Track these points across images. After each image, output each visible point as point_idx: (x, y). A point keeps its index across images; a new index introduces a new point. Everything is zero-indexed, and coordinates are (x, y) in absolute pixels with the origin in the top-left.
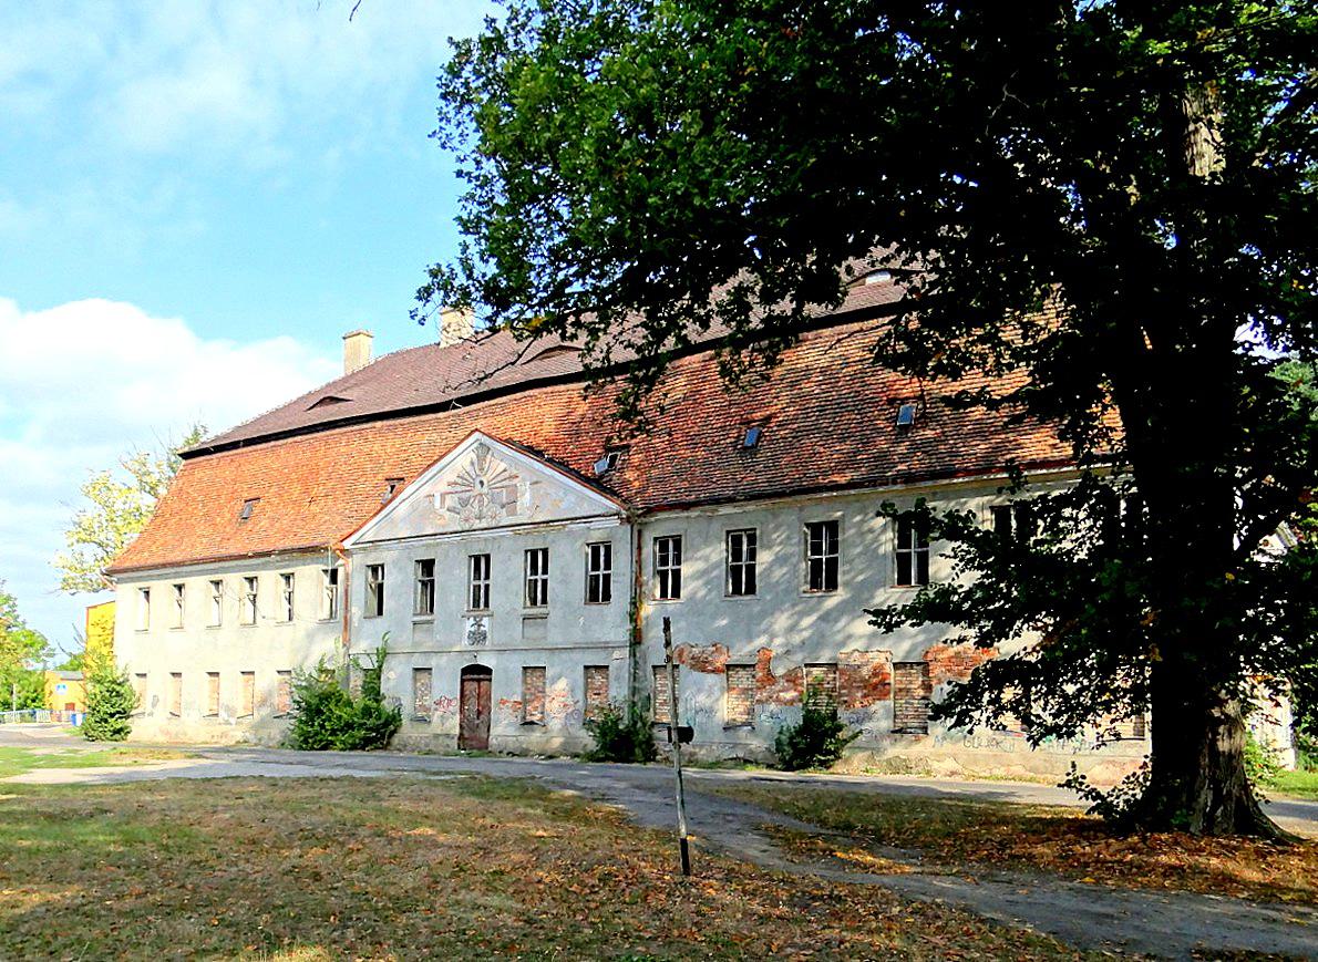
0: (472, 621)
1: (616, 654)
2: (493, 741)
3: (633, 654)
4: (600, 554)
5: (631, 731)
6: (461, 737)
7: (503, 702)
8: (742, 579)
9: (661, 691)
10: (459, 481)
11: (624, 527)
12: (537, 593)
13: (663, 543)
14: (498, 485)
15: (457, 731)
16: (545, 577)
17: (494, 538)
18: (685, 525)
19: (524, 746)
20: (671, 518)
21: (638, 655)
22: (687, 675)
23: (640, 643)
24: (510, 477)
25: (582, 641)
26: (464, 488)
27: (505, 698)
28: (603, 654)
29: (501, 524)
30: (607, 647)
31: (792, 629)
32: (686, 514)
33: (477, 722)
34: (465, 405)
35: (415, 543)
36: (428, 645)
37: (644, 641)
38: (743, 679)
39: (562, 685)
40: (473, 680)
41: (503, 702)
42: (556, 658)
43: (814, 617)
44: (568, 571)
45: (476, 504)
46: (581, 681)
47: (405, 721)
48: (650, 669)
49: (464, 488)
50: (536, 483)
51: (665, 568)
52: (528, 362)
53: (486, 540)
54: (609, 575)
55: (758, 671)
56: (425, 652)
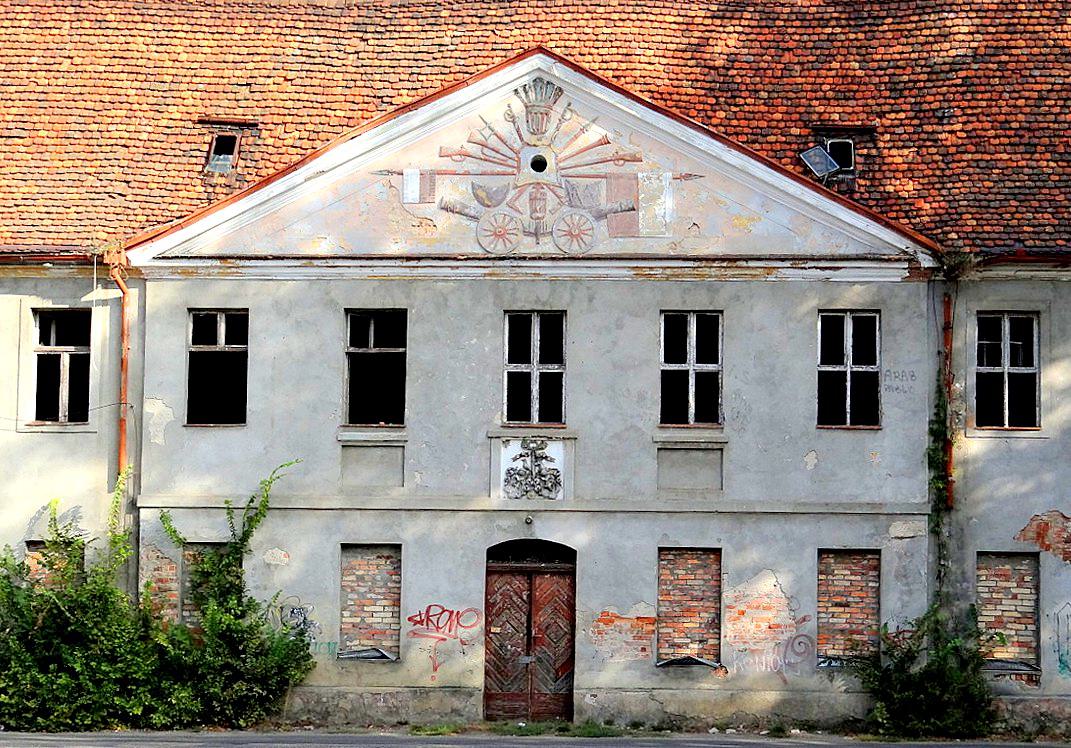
0: (515, 448)
1: (899, 528)
2: (583, 698)
3: (935, 532)
4: (849, 339)
5: (936, 674)
6: (488, 696)
7: (607, 619)
9: (989, 601)
11: (912, 285)
12: (689, 398)
13: (989, 325)
15: (478, 680)
18: (1048, 293)
20: (1016, 279)
21: (945, 531)
23: (949, 509)
24: (620, 159)
25: (813, 499)
26: (488, 167)
27: (612, 610)
28: (867, 528)
29: (593, 252)
30: (877, 514)
32: (1053, 274)
33: (527, 660)
35: (353, 270)
36: (397, 496)
37: (957, 506)
38: (253, 524)
39: (767, 586)
40: (513, 572)
41: (607, 619)
42: (749, 529)
44: (770, 363)
45: (523, 203)
46: (812, 579)
47: (320, 654)
48: (971, 561)
49: (488, 167)
50: (688, 176)
51: (997, 370)
53: (553, 281)
56: (409, 510)
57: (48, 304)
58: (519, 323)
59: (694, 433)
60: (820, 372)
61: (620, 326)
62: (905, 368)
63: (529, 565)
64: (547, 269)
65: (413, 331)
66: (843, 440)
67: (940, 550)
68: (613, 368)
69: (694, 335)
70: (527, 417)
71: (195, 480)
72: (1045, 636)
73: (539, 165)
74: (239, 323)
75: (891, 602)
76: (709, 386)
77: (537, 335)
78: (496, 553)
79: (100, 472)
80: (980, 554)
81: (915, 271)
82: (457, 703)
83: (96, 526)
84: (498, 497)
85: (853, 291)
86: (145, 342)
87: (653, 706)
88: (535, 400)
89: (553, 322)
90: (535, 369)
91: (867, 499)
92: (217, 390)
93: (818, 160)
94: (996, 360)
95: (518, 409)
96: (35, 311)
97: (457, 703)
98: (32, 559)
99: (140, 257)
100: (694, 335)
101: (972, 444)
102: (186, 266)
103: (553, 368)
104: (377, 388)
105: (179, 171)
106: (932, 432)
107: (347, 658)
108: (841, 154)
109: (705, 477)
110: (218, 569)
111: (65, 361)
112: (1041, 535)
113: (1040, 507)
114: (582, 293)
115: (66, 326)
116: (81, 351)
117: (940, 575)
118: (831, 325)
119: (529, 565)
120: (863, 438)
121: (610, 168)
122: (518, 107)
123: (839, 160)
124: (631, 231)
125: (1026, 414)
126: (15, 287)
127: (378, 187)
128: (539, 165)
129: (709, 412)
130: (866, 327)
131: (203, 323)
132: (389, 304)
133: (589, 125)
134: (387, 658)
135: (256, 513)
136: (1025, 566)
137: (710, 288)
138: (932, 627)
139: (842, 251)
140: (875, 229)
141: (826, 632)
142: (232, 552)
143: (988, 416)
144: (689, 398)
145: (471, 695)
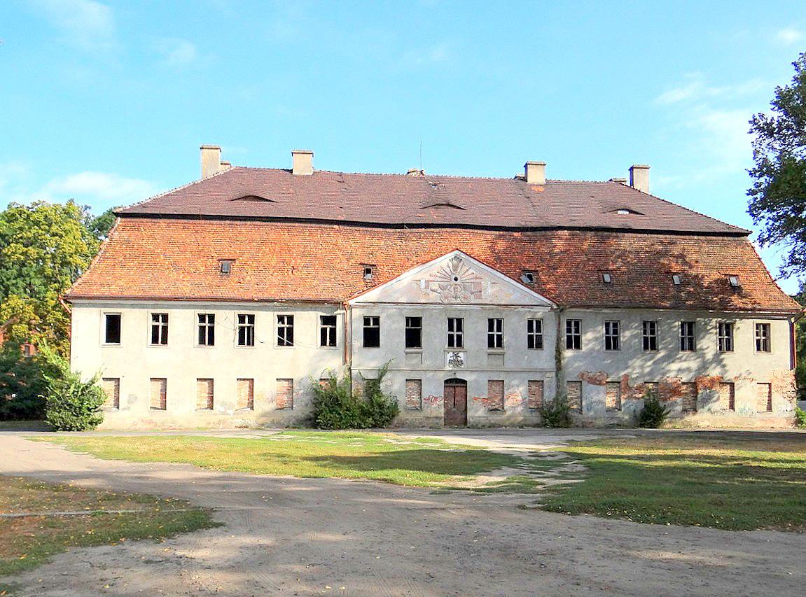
0: (451, 354)
1: (548, 375)
3: (557, 376)
4: (534, 326)
7: (476, 399)
8: (612, 343)
10: (439, 275)
12: (495, 341)
13: (569, 323)
14: (467, 281)
16: (203, 324)
17: (466, 310)
19: (492, 422)
21: (559, 375)
22: (587, 387)
24: (476, 278)
26: (442, 279)
30: (543, 371)
31: (642, 367)
33: (454, 409)
34: (409, 228)
35: (408, 306)
43: (652, 361)
44: (515, 333)
47: (400, 408)
49: (442, 279)
50: (494, 283)
52: (270, 201)
53: (460, 310)
54: (489, 331)
55: (622, 386)
57: (325, 314)
58: (451, 321)
59: (496, 350)
60: (489, 334)
61: (478, 322)
62: (549, 334)
63: (456, 384)
64: (459, 307)
65: (423, 323)
66: (534, 352)
67: (558, 380)
68: (475, 333)
69: (495, 324)
70: (453, 346)
71: (366, 362)
72: (583, 404)
73: (456, 279)
74: (376, 320)
75: (546, 394)
76: (500, 338)
77: (456, 324)
78: (446, 382)
79: (341, 360)
80: (568, 381)
81: (552, 309)
82: (437, 421)
83: (340, 377)
84: (448, 368)
85: (540, 313)
86: (351, 323)
87: (488, 421)
88: (455, 341)
89: (460, 321)
90: (495, 333)
91: (541, 367)
92: (371, 338)
93: (524, 278)
94: (571, 332)
95: (451, 344)
96: (321, 316)
97: (437, 421)
98: (323, 383)
99: (352, 302)
100: (495, 324)
101: (568, 354)
102: (363, 305)
103: (460, 333)
104: (413, 338)
105: (357, 278)
106: (556, 351)
107: (408, 410)
108: (530, 277)
109: (500, 362)
110: (373, 386)
111: (328, 330)
112: (582, 377)
113: (582, 369)
114: (467, 313)
115: (329, 320)
116: (334, 327)
117: (558, 387)
118: (530, 323)
119: (456, 384)
120: (539, 351)
121: (474, 281)
122: (451, 265)
123: (530, 278)
124: (480, 297)
125: (578, 346)
126: (316, 310)
127: (414, 285)
128: (456, 279)
129: (500, 345)
130: (539, 323)
131: (367, 321)
132: (417, 316)
133: (472, 270)
134: (419, 409)
135: (383, 372)
136: (578, 384)
137: (501, 313)
138: (556, 399)
139: (533, 304)
140: (542, 298)
141: (531, 401)
142: (379, 381)
143: (569, 346)
144: (495, 341)
145: (441, 419)
